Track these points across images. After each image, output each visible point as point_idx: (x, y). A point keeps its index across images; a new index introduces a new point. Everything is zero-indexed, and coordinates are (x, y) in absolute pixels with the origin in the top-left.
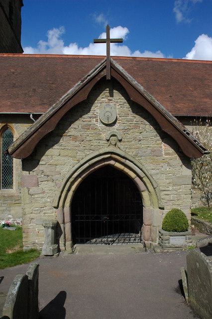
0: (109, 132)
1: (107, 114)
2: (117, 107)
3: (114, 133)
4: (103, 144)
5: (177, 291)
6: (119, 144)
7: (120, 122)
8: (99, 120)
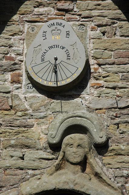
0: (61, 117)
1: (50, 56)
2: (91, 33)
3: (78, 121)
4: (36, 164)
5: (12, 157)
6: (95, 161)
7: (101, 82)
8: (24, 78)
